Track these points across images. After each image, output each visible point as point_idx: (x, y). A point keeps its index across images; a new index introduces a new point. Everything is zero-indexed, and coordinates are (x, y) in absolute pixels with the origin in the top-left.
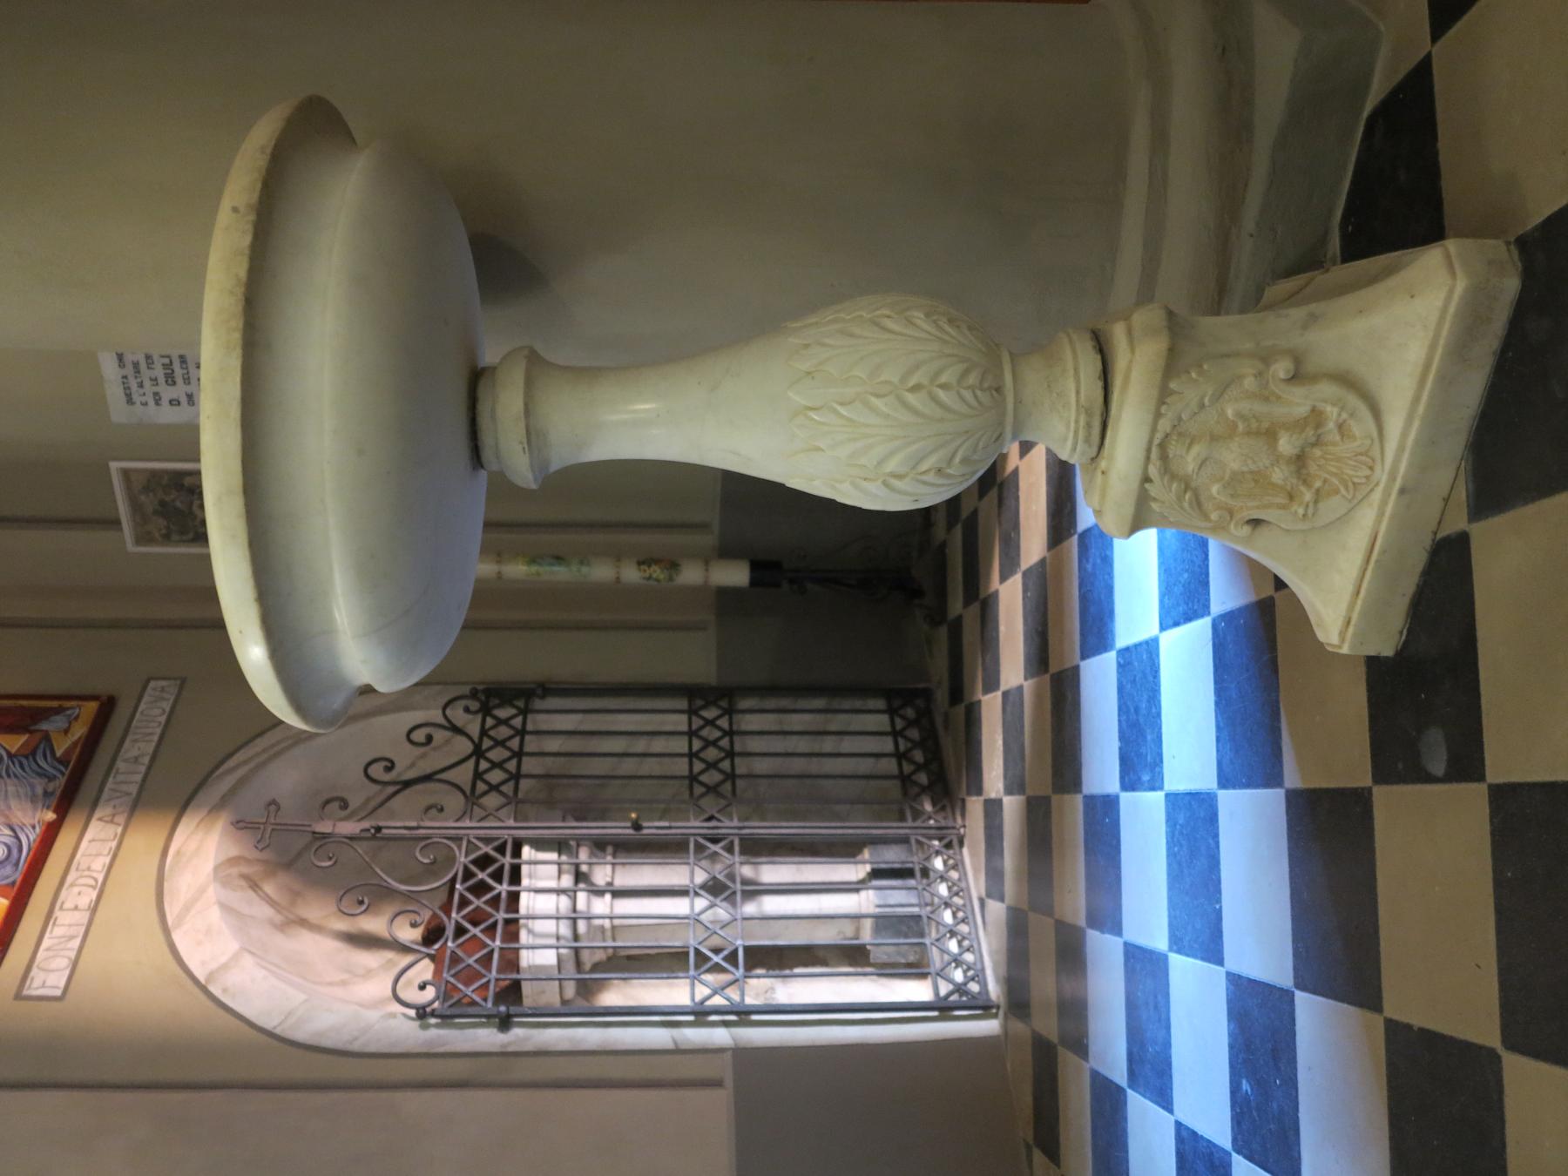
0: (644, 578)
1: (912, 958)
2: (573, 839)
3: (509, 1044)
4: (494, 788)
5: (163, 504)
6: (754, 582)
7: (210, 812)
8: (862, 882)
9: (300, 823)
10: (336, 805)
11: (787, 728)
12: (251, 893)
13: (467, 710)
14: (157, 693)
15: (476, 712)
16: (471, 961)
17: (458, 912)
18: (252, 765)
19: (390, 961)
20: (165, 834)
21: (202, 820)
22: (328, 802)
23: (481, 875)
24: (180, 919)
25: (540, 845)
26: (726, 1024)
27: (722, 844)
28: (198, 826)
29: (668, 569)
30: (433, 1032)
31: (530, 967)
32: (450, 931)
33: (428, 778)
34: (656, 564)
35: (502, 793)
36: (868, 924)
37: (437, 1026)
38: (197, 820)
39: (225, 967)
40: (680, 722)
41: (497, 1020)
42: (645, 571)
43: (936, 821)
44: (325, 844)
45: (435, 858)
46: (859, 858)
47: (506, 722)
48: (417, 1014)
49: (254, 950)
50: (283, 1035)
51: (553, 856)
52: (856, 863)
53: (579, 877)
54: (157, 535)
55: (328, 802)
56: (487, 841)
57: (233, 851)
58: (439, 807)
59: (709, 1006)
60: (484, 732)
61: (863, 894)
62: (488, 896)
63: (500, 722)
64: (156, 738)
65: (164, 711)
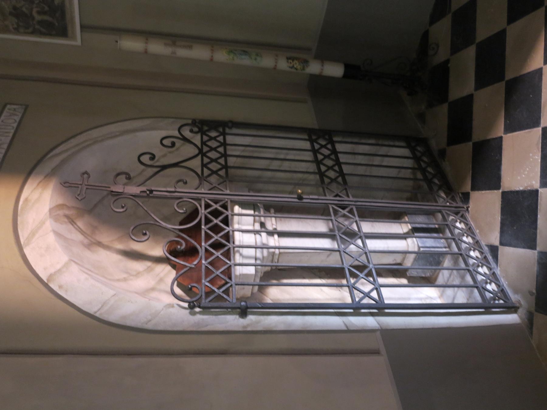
0: (290, 67)
1: (428, 275)
2: (260, 203)
3: (248, 325)
4: (213, 172)
5: (15, 8)
6: (345, 76)
7: (45, 177)
8: (407, 233)
9: (100, 185)
10: (123, 176)
11: (356, 151)
12: (71, 226)
13: (191, 131)
14: (12, 112)
15: (196, 133)
16: (218, 273)
17: (206, 242)
18: (69, 153)
19: (149, 267)
20: (17, 189)
21: (40, 182)
22: (118, 175)
23: (215, 221)
24: (29, 240)
25: (243, 205)
26: (372, 314)
27: (347, 210)
28: (38, 185)
29: (302, 63)
30: (199, 317)
31: (240, 275)
32: (202, 252)
33: (176, 165)
34: (296, 60)
35: (219, 175)
36: (412, 257)
37: (200, 313)
38: (38, 181)
39: (59, 271)
40: (307, 145)
41: (238, 310)
42: (291, 63)
43: (450, 203)
44: (117, 199)
45: (186, 210)
46: (403, 220)
47: (215, 138)
48: (189, 305)
49: (76, 261)
50: (101, 317)
51: (251, 212)
52: (400, 223)
53: (262, 225)
54: (11, 28)
55: (118, 175)
56: (216, 202)
57: (60, 201)
58: (185, 181)
59: (363, 304)
60: (203, 143)
61: (409, 240)
62: (222, 234)
63: (211, 138)
64: (11, 135)
65: (16, 121)
